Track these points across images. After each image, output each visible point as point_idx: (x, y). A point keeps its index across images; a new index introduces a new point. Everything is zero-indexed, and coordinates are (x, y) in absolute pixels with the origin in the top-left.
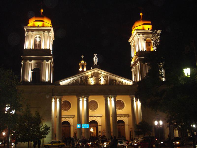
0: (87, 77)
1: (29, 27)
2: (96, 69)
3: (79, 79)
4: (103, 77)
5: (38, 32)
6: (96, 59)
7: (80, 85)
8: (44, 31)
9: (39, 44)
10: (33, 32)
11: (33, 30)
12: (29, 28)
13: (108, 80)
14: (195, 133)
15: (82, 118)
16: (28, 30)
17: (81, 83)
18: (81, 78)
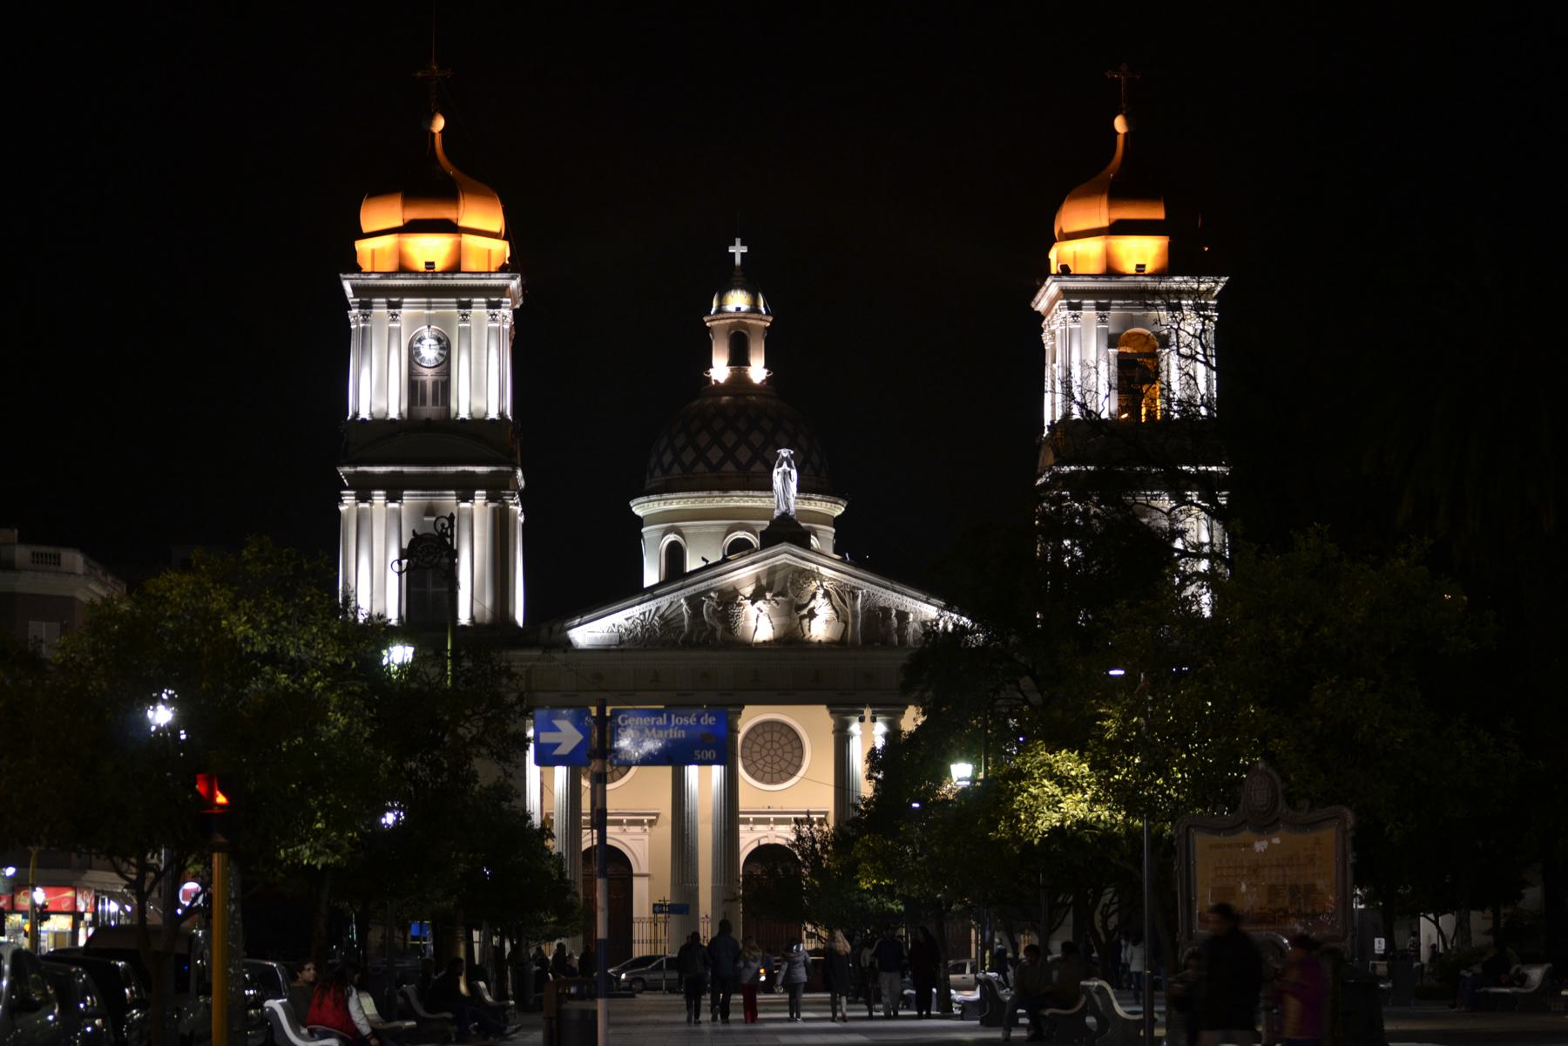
0: (729, 598)
1: (373, 276)
2: (784, 547)
3: (685, 607)
4: (827, 594)
5: (429, 308)
6: (784, 480)
7: (689, 643)
8: (464, 296)
9: (435, 383)
10: (398, 305)
11: (394, 297)
12: (374, 281)
13: (855, 615)
14: (1376, 946)
15: (696, 828)
16: (367, 294)
17: (691, 631)
18: (695, 602)
